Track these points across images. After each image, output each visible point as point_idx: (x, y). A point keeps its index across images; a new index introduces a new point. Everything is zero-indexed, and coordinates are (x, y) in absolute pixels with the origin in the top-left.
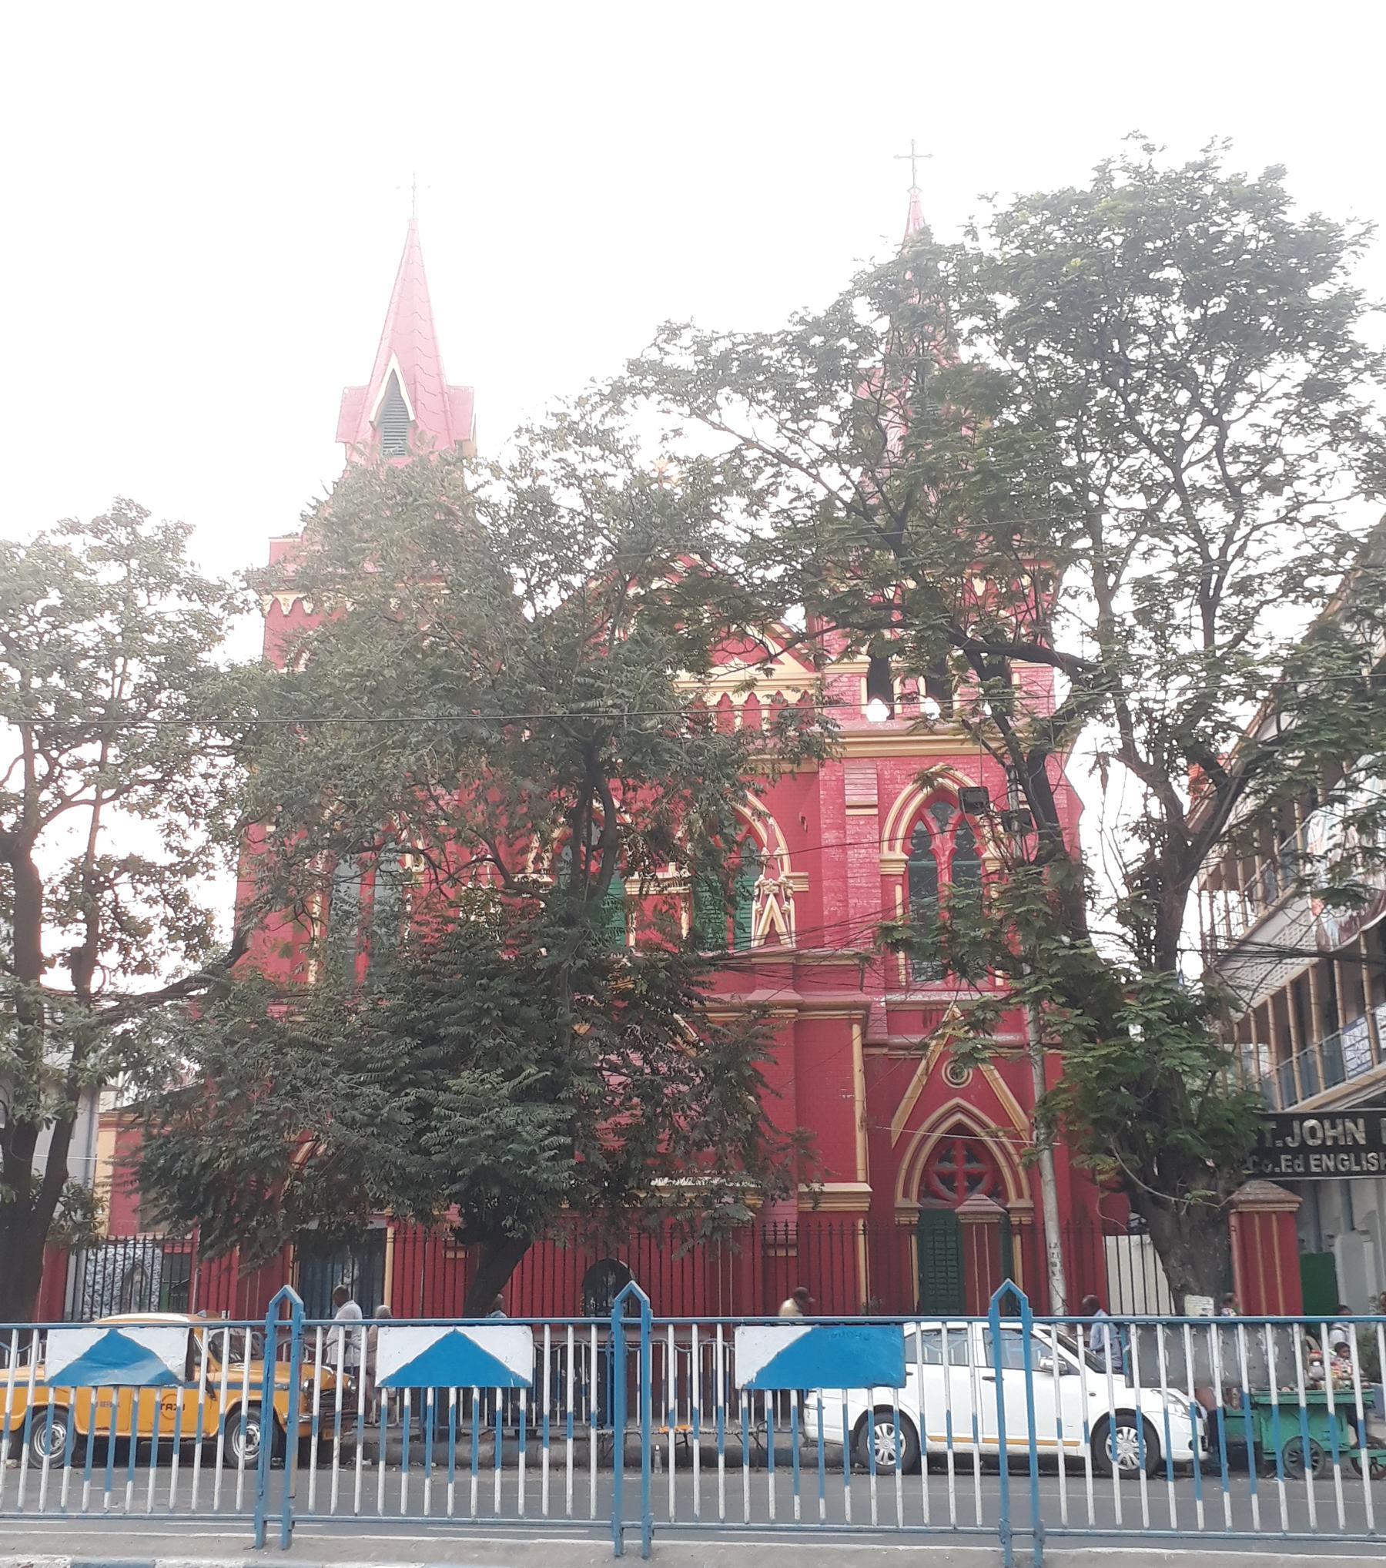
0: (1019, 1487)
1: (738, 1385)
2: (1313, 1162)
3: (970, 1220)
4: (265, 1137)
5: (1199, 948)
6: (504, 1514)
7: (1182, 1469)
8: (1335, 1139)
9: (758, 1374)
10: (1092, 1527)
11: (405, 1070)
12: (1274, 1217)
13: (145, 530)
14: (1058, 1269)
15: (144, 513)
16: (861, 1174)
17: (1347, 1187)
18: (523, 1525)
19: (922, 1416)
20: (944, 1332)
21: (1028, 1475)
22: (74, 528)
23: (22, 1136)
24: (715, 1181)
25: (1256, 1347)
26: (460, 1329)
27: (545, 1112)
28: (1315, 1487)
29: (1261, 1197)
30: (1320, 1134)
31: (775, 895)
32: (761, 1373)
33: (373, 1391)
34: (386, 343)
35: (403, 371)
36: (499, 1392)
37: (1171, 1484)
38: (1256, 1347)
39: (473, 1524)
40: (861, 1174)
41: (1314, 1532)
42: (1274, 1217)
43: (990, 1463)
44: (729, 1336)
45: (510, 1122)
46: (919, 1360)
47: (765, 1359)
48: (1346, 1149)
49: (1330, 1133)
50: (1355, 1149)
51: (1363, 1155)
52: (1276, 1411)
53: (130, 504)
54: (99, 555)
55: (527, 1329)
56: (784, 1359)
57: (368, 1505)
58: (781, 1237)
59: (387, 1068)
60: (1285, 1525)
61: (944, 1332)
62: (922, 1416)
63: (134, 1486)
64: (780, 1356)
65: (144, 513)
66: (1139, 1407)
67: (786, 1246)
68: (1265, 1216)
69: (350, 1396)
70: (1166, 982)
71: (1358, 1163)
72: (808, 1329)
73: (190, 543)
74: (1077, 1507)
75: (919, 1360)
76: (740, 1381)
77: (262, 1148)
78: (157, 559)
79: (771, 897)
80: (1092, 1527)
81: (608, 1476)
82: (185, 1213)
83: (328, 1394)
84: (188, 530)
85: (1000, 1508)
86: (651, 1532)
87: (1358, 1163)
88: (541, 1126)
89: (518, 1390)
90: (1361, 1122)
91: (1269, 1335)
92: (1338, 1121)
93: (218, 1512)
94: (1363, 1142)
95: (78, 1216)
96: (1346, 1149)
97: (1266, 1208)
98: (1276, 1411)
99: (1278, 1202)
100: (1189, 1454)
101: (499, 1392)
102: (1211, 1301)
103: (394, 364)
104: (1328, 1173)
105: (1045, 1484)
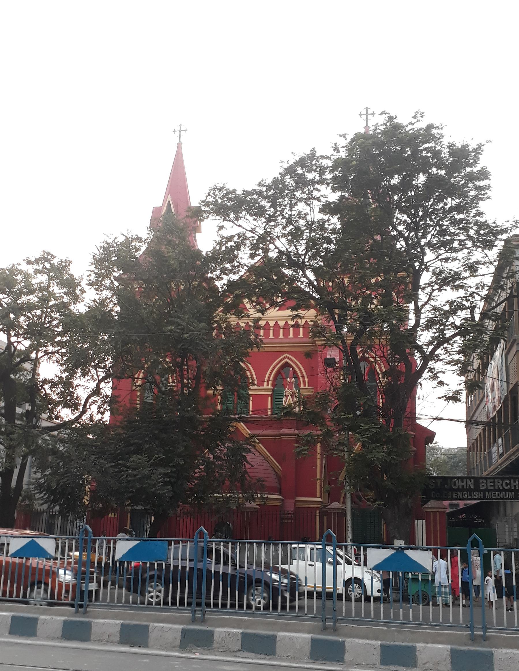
0: (329, 604)
1: (116, 560)
2: (493, 495)
3: (331, 511)
4: (68, 476)
5: (464, 418)
6: (394, 619)
7: (377, 599)
8: (463, 486)
9: (123, 556)
10: (441, 623)
11: (119, 454)
12: (438, 513)
13: (56, 262)
14: (350, 528)
15: (54, 257)
16: (318, 494)
17: (505, 503)
18: (422, 625)
19: (306, 578)
20: (315, 549)
21: (321, 599)
22: (29, 262)
23: (7, 474)
24: (228, 495)
25: (276, 551)
26: (35, 539)
27: (161, 470)
28: (422, 608)
29: (433, 506)
30: (457, 484)
31: (291, 395)
32: (124, 556)
33: (114, 562)
34: (168, 190)
35: (174, 202)
36: (125, 563)
37: (382, 605)
38: (276, 551)
39: (178, 609)
40: (318, 494)
41: (451, 623)
42: (438, 513)
43: (320, 595)
44: (115, 543)
45: (147, 473)
46: (315, 561)
47: (125, 551)
48: (466, 490)
49: (461, 484)
50: (470, 490)
51: (472, 492)
52: (410, 580)
53: (48, 254)
54: (37, 272)
55: (54, 539)
56: (131, 551)
57: (112, 600)
58: (286, 516)
59: (112, 454)
60: (401, 619)
61: (315, 549)
62: (306, 578)
63: (403, 610)
64: (129, 550)
65: (54, 257)
66: (363, 578)
67: (288, 519)
68: (435, 513)
69: (107, 564)
70: (371, 428)
71: (471, 495)
72: (139, 542)
73: (72, 267)
74: (349, 612)
75: (315, 561)
76: (117, 558)
77: (68, 480)
78: (59, 272)
79: (290, 396)
80: (441, 623)
81: (321, 602)
82: (54, 501)
83: (100, 563)
84: (70, 262)
85: (322, 609)
86: (336, 621)
87: (471, 495)
88: (160, 474)
89: (124, 562)
90: (473, 481)
91: (280, 548)
92: (465, 480)
93: (108, 603)
94: (472, 488)
95: (27, 502)
96: (466, 490)
97: (435, 510)
98: (410, 580)
99: (438, 508)
100: (378, 594)
101: (125, 563)
102: (404, 542)
103: (169, 198)
104: (501, 499)
105: (339, 603)
